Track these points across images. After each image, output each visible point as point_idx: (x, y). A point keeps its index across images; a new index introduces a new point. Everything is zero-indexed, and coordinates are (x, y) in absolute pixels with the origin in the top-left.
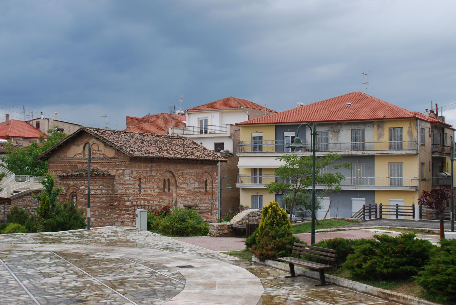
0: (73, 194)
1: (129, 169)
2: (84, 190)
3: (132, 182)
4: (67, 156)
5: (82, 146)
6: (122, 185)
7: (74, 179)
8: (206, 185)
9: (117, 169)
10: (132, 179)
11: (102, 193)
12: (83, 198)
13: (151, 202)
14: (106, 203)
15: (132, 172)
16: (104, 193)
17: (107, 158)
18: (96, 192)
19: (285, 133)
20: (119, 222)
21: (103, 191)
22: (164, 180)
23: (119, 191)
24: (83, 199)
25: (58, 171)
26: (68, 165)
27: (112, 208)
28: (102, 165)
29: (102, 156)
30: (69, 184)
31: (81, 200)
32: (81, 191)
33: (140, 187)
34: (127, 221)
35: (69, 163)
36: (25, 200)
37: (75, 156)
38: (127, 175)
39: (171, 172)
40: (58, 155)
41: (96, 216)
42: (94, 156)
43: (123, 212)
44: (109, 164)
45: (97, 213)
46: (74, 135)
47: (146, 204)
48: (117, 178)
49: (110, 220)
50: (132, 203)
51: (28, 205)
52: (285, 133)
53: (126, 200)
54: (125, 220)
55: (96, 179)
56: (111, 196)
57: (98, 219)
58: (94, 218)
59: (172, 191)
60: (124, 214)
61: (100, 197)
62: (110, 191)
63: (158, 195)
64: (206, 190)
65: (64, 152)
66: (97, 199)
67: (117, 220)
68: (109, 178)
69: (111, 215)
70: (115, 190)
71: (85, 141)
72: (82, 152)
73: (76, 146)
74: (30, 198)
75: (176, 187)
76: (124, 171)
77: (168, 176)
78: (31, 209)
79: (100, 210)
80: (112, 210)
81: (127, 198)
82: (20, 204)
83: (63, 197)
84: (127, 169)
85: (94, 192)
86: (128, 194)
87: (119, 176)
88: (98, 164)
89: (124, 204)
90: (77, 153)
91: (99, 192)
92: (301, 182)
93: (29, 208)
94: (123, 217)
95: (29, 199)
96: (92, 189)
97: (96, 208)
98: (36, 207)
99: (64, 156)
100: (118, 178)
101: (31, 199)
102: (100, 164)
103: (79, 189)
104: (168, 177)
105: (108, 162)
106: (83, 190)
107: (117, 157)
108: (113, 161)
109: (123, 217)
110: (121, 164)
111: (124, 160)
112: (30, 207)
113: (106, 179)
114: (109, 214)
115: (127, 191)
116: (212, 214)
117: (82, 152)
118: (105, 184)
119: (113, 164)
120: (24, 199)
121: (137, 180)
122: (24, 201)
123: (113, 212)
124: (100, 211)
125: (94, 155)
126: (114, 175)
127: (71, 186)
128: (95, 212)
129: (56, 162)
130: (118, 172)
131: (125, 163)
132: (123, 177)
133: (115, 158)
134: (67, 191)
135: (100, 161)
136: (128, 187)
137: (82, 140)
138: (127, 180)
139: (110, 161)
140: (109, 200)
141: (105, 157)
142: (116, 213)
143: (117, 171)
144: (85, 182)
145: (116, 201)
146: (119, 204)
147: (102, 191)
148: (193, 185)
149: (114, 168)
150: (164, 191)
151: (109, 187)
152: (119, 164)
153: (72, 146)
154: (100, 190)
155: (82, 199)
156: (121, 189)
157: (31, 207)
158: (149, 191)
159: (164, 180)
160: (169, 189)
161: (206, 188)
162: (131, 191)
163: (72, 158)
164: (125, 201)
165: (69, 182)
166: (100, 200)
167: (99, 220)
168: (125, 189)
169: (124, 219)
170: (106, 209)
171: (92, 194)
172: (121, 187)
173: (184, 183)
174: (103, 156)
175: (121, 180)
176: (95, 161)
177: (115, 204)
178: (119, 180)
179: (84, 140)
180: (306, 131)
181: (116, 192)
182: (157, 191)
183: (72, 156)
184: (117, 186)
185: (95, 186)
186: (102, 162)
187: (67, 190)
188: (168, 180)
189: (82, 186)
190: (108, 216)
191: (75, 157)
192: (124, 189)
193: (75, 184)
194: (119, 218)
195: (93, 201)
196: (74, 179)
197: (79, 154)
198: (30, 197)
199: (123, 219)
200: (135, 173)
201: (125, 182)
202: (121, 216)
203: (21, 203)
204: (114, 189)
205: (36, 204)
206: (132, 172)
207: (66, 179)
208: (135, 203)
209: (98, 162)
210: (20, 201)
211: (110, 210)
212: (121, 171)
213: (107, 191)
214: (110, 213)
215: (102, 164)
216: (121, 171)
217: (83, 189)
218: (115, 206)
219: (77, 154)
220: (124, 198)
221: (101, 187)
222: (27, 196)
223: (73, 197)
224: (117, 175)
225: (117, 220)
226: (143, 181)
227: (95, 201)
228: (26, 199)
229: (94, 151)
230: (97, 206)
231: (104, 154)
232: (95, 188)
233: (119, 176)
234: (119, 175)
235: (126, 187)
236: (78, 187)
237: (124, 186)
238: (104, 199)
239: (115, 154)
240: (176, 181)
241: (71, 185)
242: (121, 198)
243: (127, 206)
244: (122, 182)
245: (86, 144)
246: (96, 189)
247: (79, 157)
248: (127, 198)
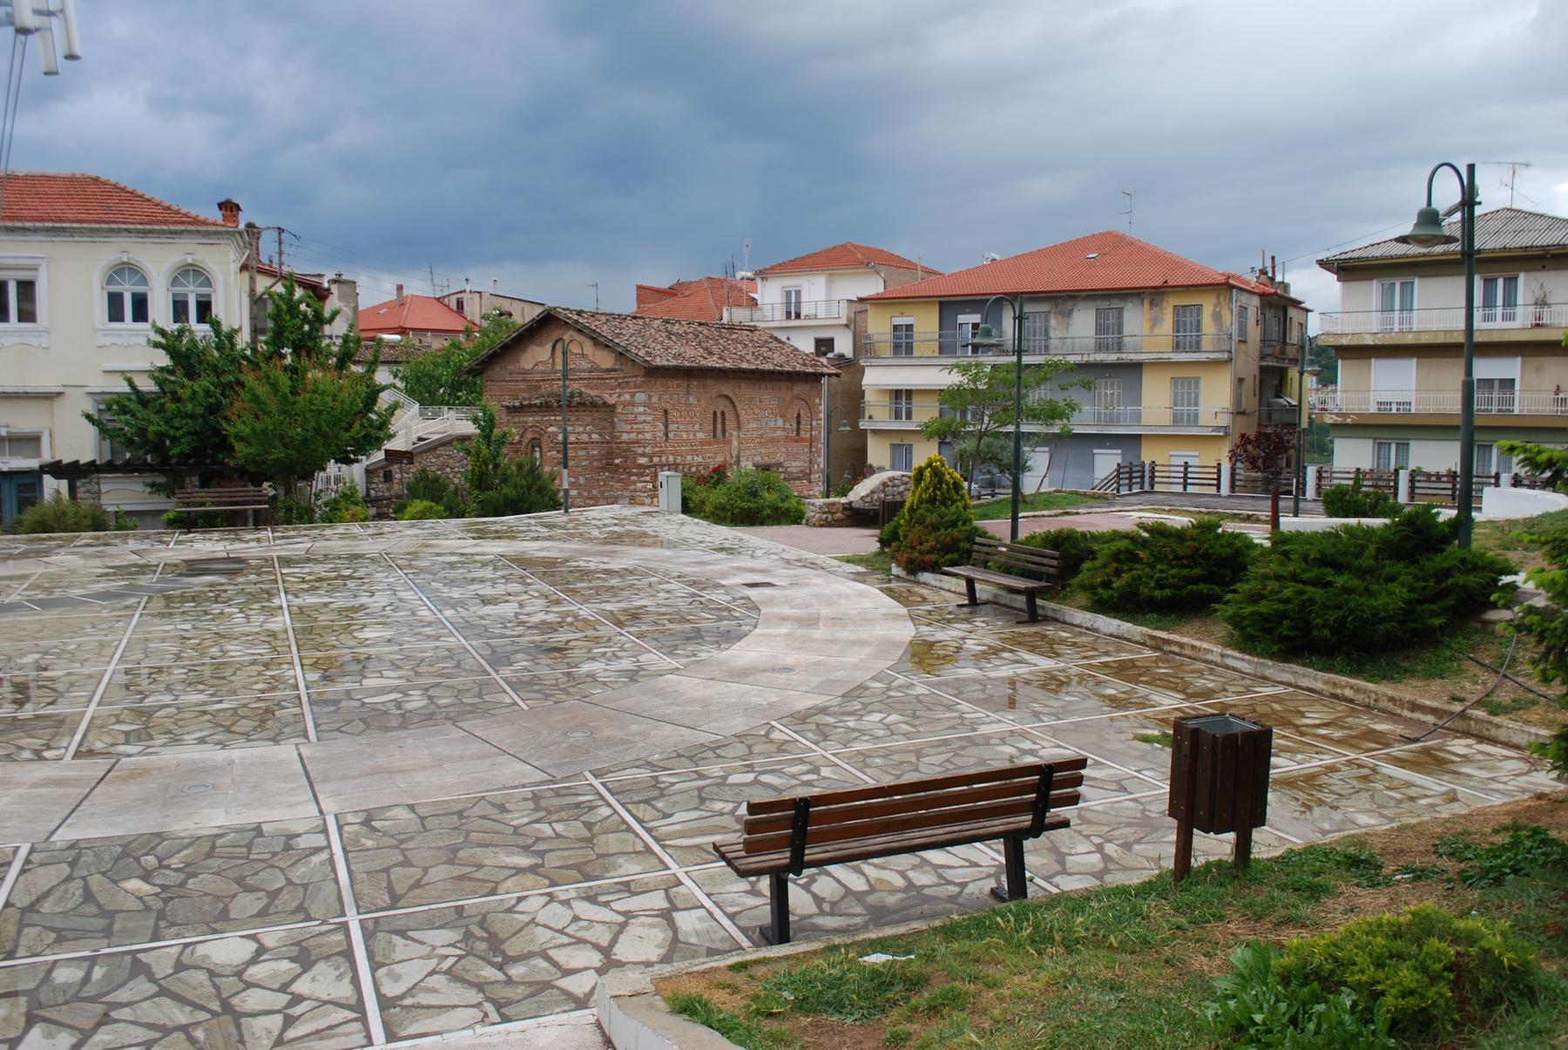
3: (649, 418)
5: (549, 347)
8: (799, 423)
10: (649, 411)
13: (690, 458)
14: (600, 460)
15: (650, 398)
21: (594, 436)
22: (715, 413)
23: (625, 437)
29: (589, 366)
33: (666, 428)
36: (441, 455)
38: (640, 405)
39: (727, 397)
47: (678, 461)
50: (651, 461)
59: (731, 435)
60: (635, 483)
63: (703, 443)
64: (798, 434)
71: (555, 335)
75: (739, 428)
76: (633, 395)
77: (722, 405)
81: (640, 450)
91: (584, 437)
93: (448, 470)
104: (722, 408)
115: (641, 436)
116: (810, 482)
118: (596, 422)
121: (660, 414)
122: (439, 456)
133: (615, 370)
138: (641, 414)
143: (620, 395)
148: (772, 424)
150: (715, 436)
158: (685, 436)
159: (715, 413)
160: (724, 431)
161: (798, 430)
162: (648, 436)
164: (636, 455)
172: (629, 427)
173: (754, 419)
177: (617, 461)
182: (701, 435)
184: (621, 426)
188: (723, 413)
200: (655, 399)
206: (650, 398)
208: (656, 460)
212: (627, 397)
216: (627, 397)
223: (533, 447)
226: (673, 414)
234: (625, 404)
240: (737, 415)
242: (629, 450)
244: (630, 417)
248: (640, 450)
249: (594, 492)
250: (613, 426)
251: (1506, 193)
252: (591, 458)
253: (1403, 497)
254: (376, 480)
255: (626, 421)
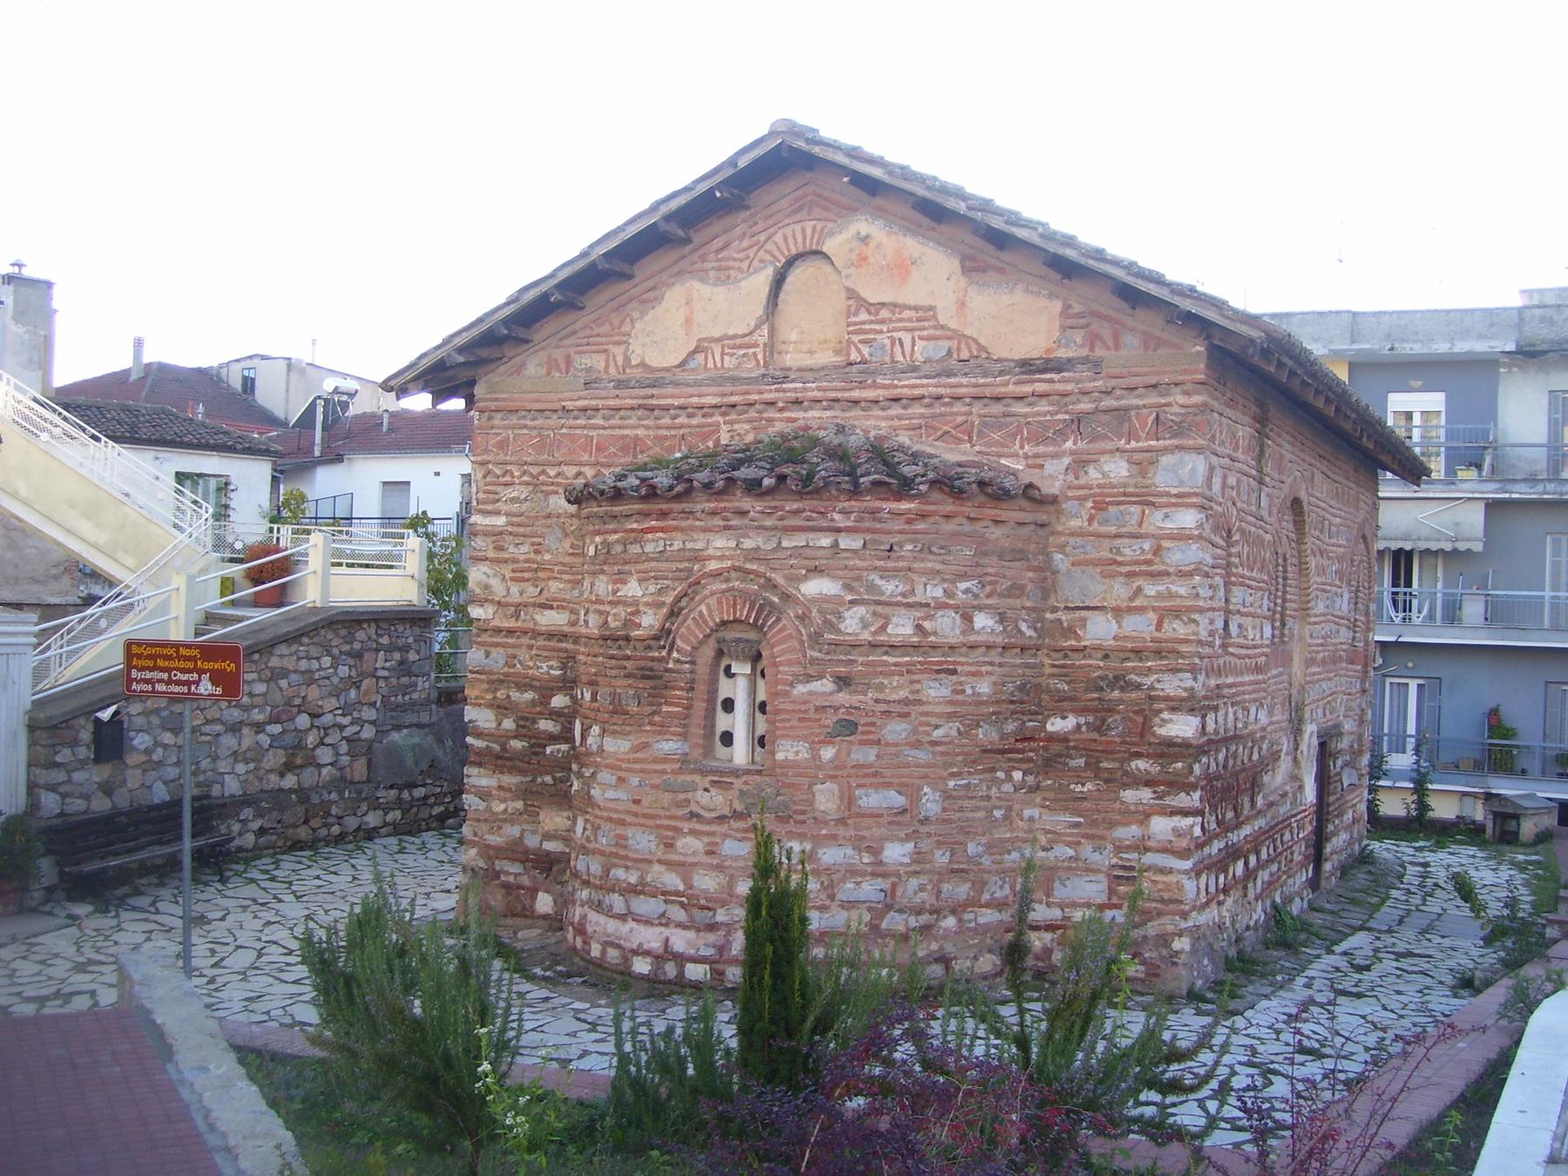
0: (730, 635)
1: (1198, 450)
2: (831, 609)
4: (627, 359)
5: (760, 282)
6: (1131, 575)
7: (744, 513)
9: (1081, 445)
11: (972, 638)
12: (820, 677)
14: (997, 718)
16: (980, 638)
17: (980, 361)
18: (927, 625)
19: (1392, 397)
20: (1089, 870)
23: (1099, 629)
24: (826, 685)
25: (552, 473)
26: (632, 422)
27: (1030, 760)
28: (934, 416)
29: (938, 350)
30: (698, 557)
31: (801, 689)
32: (803, 618)
34: (1171, 871)
35: (640, 407)
36: (284, 673)
37: (700, 358)
38: (1181, 500)
40: (558, 354)
41: (925, 821)
42: (866, 350)
43: (1129, 795)
44: (997, 409)
45: (931, 803)
46: (711, 190)
48: (1076, 518)
49: (1015, 855)
51: (297, 701)
52: (1392, 397)
53: (1167, 699)
54: (1149, 859)
55: (923, 516)
56: (1027, 666)
57: (939, 844)
58: (907, 838)
60: (1145, 816)
61: (954, 672)
62: (1024, 627)
65: (606, 328)
66: (936, 691)
67: (1071, 852)
68: (1021, 516)
69: (1027, 813)
70: (1064, 617)
71: (791, 236)
72: (757, 327)
73: (703, 281)
74: (309, 658)
76: (1143, 464)
78: (312, 726)
79: (953, 775)
80: (1030, 779)
82: (251, 695)
83: (629, 664)
84: (1180, 448)
85: (909, 630)
86: (1183, 648)
87: (1100, 506)
88: (896, 410)
89: (1146, 727)
90: (717, 334)
91: (946, 626)
92: (1067, 638)
93: (303, 721)
94: (1130, 832)
95: (303, 665)
96: (898, 604)
97: (922, 756)
98: (343, 715)
99: (603, 357)
100: (1091, 520)
101: (315, 665)
102: (918, 409)
103: (786, 597)
105: (988, 392)
106: (820, 612)
107: (1084, 352)
108: (1041, 387)
109: (1130, 832)
110: (1121, 413)
111: (1153, 380)
112: (314, 716)
113: (996, 522)
114: (1009, 809)
117: (757, 327)
118: (992, 566)
119: (1043, 406)
120: (275, 662)
122: (276, 675)
123: (1037, 788)
124: (951, 784)
125: (863, 342)
126: (1053, 500)
127: (716, 575)
128: (914, 796)
129: (538, 406)
130: (1093, 475)
131: (1154, 399)
132: (1135, 509)
133: (1055, 366)
134: (673, 614)
135: (917, 392)
136: (1182, 591)
137: (762, 237)
139: (1011, 388)
140: (1018, 696)
141: (965, 355)
142: (1072, 802)
143: (1080, 463)
144: (846, 542)
145: (1061, 705)
146: (1100, 727)
147: (968, 618)
149: (1045, 441)
151: (1017, 590)
152: (1096, 411)
153: (669, 286)
154: (956, 608)
155: (816, 686)
156: (1118, 612)
157: (319, 716)
163: (667, 370)
165: (699, 545)
166: (956, 692)
167: (945, 859)
168: (1154, 609)
169: (1142, 847)
170: (993, 770)
171: (895, 641)
172: (1119, 591)
174: (949, 353)
175: (1118, 536)
176: (875, 386)
178: (1099, 536)
179: (778, 238)
180: (1501, 390)
181: (1070, 631)
183: (674, 359)
185: (919, 581)
186: (939, 398)
187: (678, 599)
189: (816, 571)
190: (1006, 817)
191: (692, 365)
192: (1141, 610)
193: (754, 555)
194: (1092, 837)
195: (906, 702)
196: (744, 513)
197: (735, 337)
198: (314, 652)
199: (1128, 849)
201: (1157, 550)
202: (1113, 825)
203: (260, 688)
204: (1055, 610)
205: (342, 698)
207: (663, 515)
209: (896, 400)
210: (254, 676)
211: (1018, 775)
212: (1118, 469)
213: (1002, 619)
214: (1017, 796)
215: (938, 409)
217: (824, 599)
218: (1052, 738)
219: (718, 340)
220: (1147, 681)
221: (963, 585)
222: (294, 648)
224: (1085, 498)
225: (1071, 852)
227: (920, 702)
228: (290, 664)
229: (863, 316)
230: (934, 743)
231: (960, 336)
232: (919, 598)
233: (1100, 506)
235: (1172, 595)
236: (778, 578)
237: (1151, 589)
238: (984, 688)
239: (1063, 328)
241: (713, 565)
242: (1120, 682)
243: (1171, 749)
244: (1130, 549)
245: (790, 263)
246: (928, 605)
247: (729, 362)
248: (1171, 686)
249: (972, 848)
250: (1047, 583)
251: (1449, 345)
252: (969, 714)
253: (1413, 685)
254: (64, 755)
255: (1109, 567)
